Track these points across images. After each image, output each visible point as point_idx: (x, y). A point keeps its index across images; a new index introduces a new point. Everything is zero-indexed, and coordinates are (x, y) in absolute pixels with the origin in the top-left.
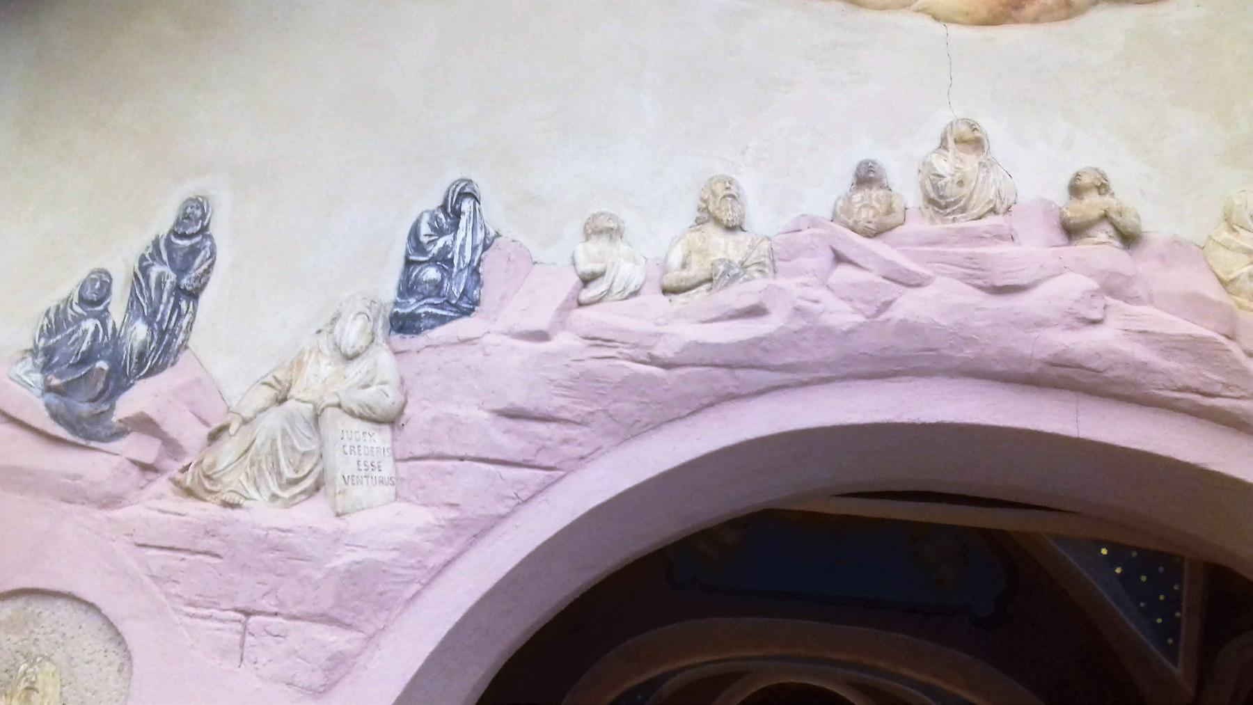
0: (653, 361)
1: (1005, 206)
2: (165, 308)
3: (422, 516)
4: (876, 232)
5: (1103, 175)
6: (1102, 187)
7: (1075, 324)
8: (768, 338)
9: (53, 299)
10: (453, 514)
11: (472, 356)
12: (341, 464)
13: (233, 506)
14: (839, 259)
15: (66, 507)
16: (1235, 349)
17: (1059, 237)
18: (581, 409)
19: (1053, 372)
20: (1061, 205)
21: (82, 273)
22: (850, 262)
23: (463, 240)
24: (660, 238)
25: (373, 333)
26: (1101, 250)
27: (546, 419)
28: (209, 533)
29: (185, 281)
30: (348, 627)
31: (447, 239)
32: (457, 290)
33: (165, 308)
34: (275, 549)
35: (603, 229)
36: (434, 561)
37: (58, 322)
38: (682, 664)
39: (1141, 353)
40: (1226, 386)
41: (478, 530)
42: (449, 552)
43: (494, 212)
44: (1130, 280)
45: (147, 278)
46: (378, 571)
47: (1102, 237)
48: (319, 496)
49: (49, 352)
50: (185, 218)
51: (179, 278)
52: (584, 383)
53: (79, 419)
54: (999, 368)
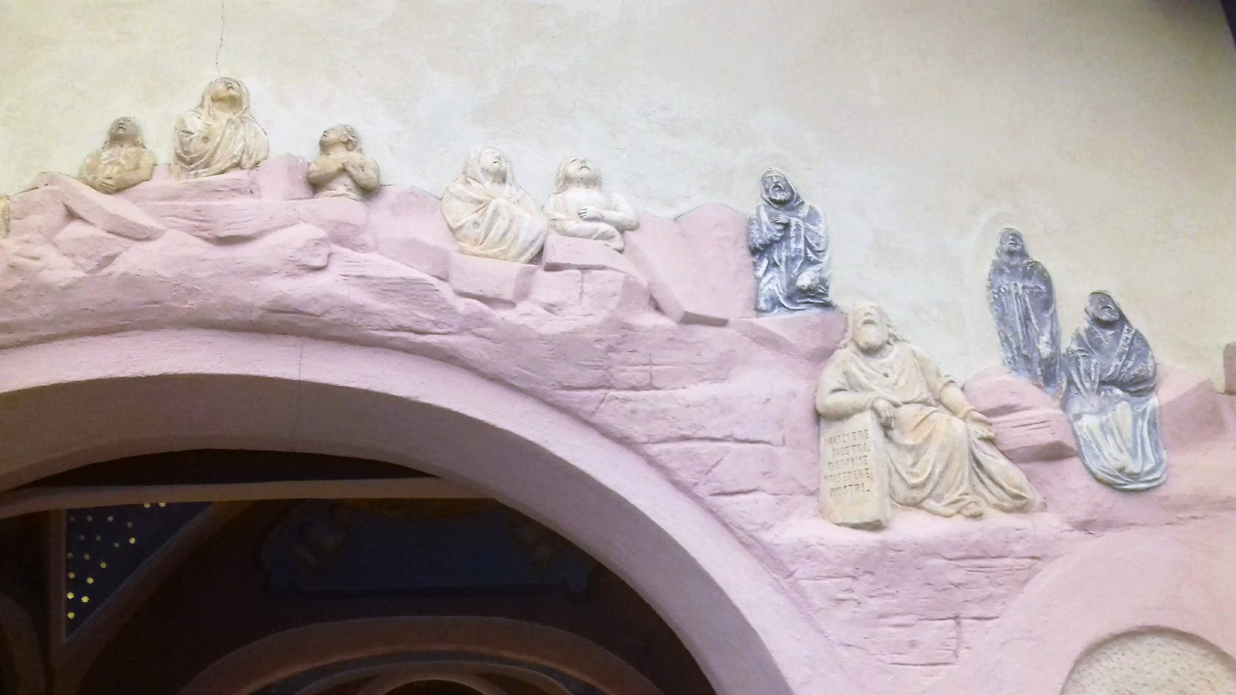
1: (252, 161)
4: (118, 189)
5: (351, 132)
6: (350, 143)
7: (297, 271)
14: (71, 215)
16: (445, 290)
17: (302, 190)
19: (275, 317)
20: (308, 160)
22: (80, 218)
26: (339, 203)
39: (358, 296)
40: (435, 323)
44: (358, 229)
47: (341, 189)
54: (223, 317)
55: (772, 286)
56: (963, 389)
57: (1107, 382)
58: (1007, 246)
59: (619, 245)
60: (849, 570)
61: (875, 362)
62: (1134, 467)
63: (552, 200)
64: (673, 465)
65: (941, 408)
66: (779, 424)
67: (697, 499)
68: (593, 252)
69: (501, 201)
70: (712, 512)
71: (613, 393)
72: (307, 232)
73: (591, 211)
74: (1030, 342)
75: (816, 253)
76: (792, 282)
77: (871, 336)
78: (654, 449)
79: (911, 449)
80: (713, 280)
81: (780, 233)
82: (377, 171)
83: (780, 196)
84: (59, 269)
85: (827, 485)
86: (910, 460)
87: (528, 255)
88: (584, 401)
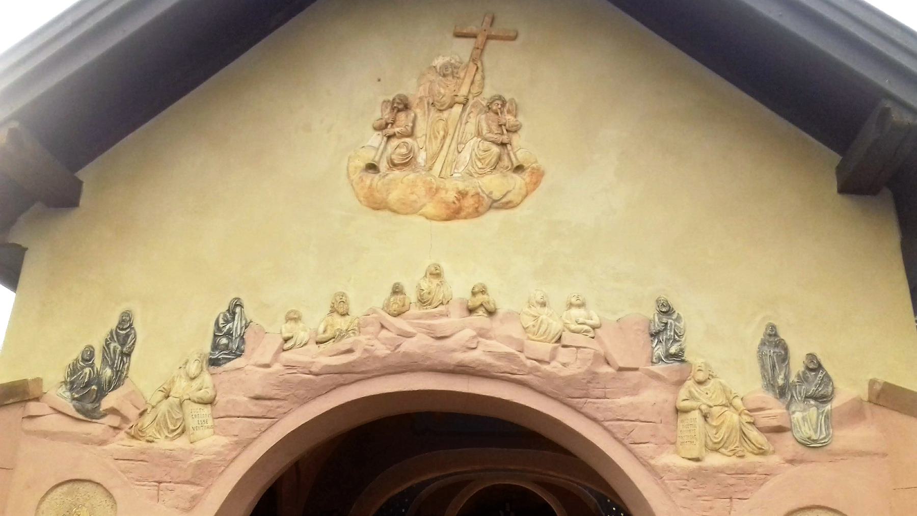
0: (311, 373)
2: (117, 362)
3: (224, 440)
4: (398, 314)
5: (484, 287)
6: (483, 292)
8: (354, 362)
9: (70, 360)
10: (236, 439)
11: (242, 375)
12: (191, 423)
13: (151, 442)
14: (383, 327)
15: (85, 446)
16: (522, 356)
17: (466, 313)
18: (283, 394)
21: (82, 347)
23: (237, 324)
24: (318, 319)
25: (202, 367)
26: (480, 319)
27: (270, 399)
28: (142, 453)
29: (125, 349)
30: (198, 485)
31: (230, 325)
32: (235, 347)
33: (117, 362)
34: (168, 457)
35: (293, 318)
36: (228, 458)
37: (74, 370)
38: (452, 471)
39: (489, 360)
40: (519, 370)
41: (244, 445)
42: (234, 454)
43: (250, 311)
44: (488, 331)
45: (109, 349)
46: (208, 463)
47: (481, 313)
48: (184, 435)
49: (72, 383)
50: (122, 321)
51: (122, 348)
52: (284, 384)
53: (88, 411)
55: (659, 352)
56: (742, 399)
57: (807, 397)
58: (768, 331)
59: (591, 335)
60: (686, 477)
61: (702, 388)
62: (814, 437)
63: (565, 313)
64: (614, 431)
65: (732, 408)
66: (659, 414)
67: (624, 445)
68: (581, 340)
69: (544, 317)
70: (630, 451)
71: (589, 400)
72: (469, 333)
73: (581, 320)
74: (774, 377)
75: (679, 336)
76: (667, 351)
77: (701, 376)
78: (606, 424)
79: (715, 427)
80: (631, 351)
81: (664, 327)
82: (494, 304)
83: (664, 310)
84: (382, 350)
85: (679, 440)
86: (714, 431)
87: (554, 340)
88: (578, 403)
